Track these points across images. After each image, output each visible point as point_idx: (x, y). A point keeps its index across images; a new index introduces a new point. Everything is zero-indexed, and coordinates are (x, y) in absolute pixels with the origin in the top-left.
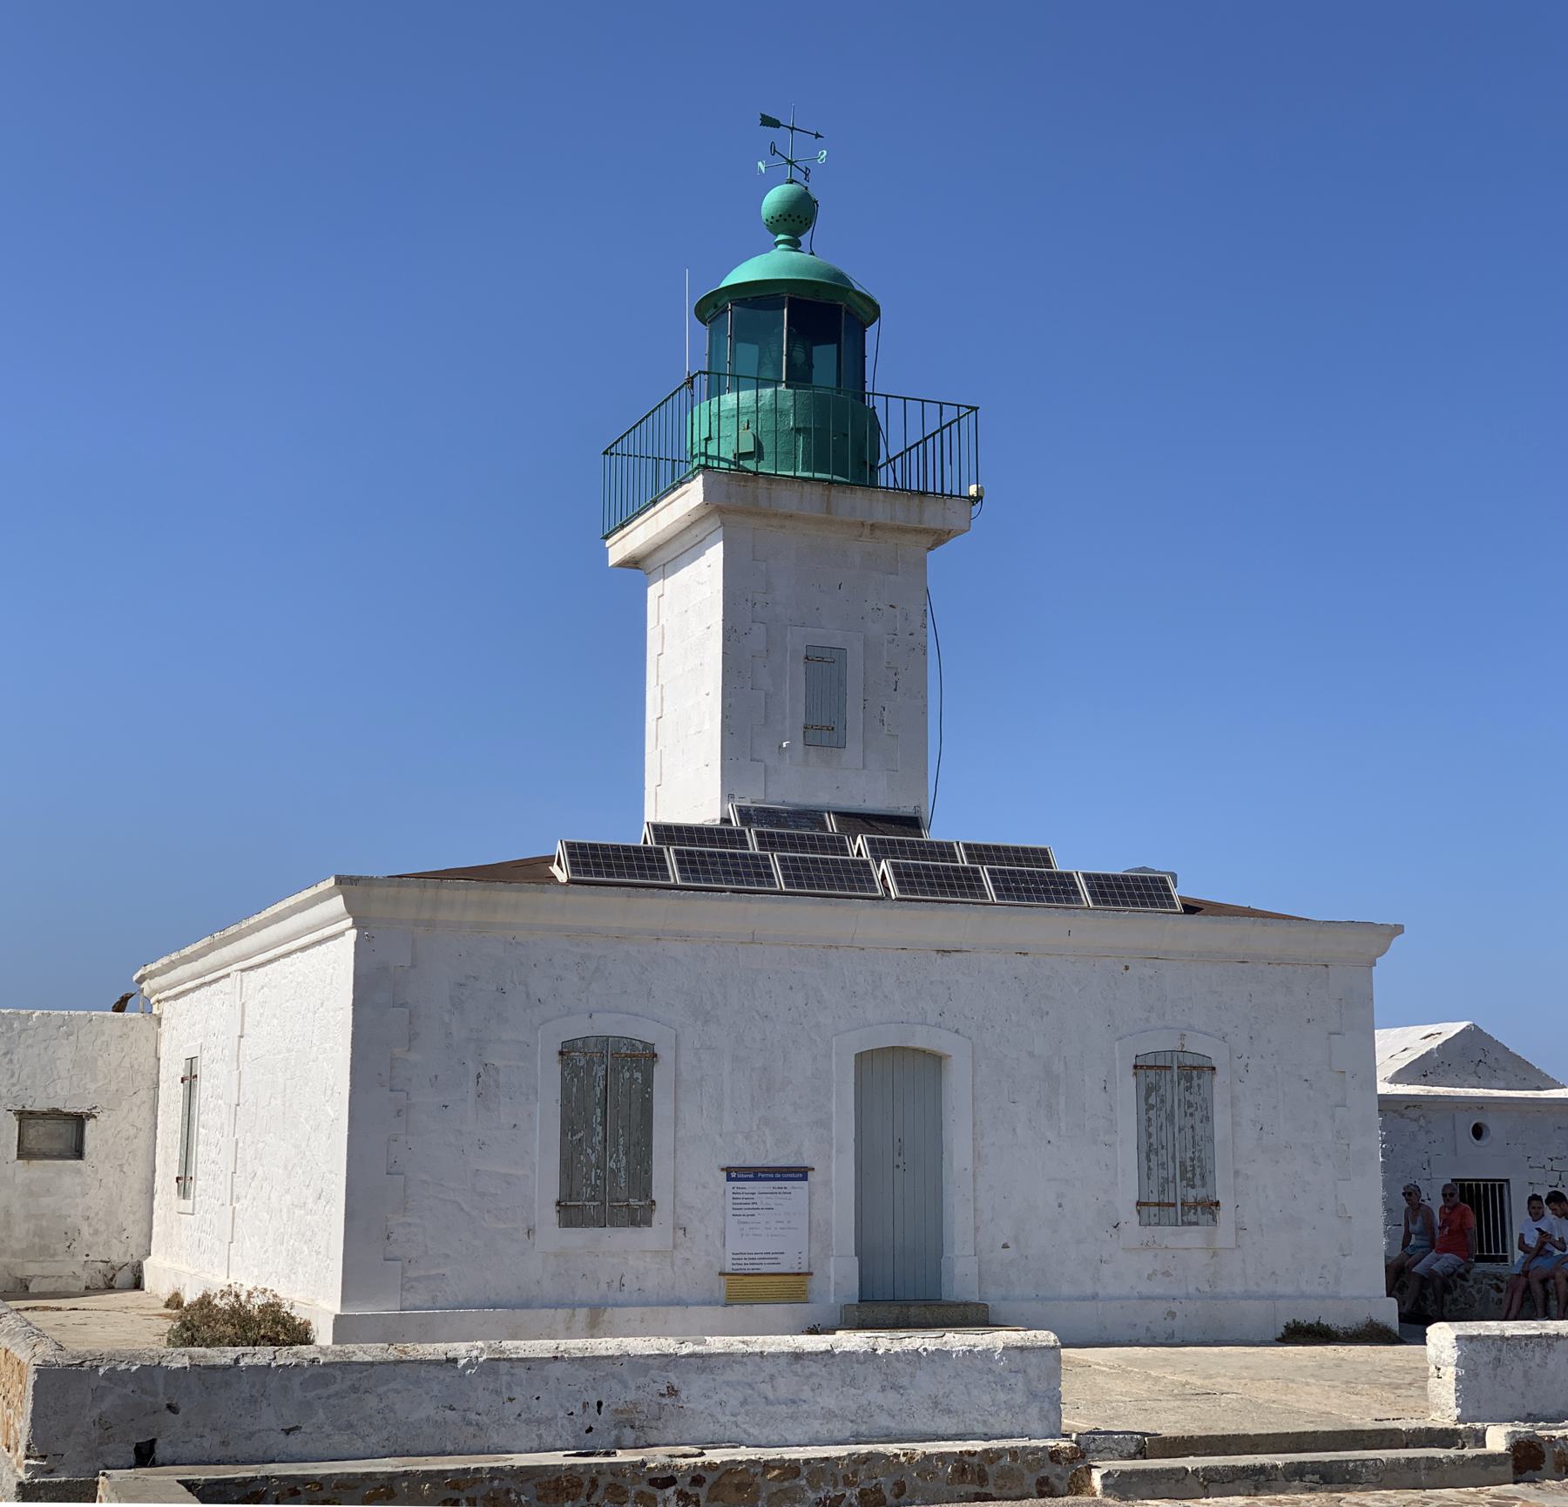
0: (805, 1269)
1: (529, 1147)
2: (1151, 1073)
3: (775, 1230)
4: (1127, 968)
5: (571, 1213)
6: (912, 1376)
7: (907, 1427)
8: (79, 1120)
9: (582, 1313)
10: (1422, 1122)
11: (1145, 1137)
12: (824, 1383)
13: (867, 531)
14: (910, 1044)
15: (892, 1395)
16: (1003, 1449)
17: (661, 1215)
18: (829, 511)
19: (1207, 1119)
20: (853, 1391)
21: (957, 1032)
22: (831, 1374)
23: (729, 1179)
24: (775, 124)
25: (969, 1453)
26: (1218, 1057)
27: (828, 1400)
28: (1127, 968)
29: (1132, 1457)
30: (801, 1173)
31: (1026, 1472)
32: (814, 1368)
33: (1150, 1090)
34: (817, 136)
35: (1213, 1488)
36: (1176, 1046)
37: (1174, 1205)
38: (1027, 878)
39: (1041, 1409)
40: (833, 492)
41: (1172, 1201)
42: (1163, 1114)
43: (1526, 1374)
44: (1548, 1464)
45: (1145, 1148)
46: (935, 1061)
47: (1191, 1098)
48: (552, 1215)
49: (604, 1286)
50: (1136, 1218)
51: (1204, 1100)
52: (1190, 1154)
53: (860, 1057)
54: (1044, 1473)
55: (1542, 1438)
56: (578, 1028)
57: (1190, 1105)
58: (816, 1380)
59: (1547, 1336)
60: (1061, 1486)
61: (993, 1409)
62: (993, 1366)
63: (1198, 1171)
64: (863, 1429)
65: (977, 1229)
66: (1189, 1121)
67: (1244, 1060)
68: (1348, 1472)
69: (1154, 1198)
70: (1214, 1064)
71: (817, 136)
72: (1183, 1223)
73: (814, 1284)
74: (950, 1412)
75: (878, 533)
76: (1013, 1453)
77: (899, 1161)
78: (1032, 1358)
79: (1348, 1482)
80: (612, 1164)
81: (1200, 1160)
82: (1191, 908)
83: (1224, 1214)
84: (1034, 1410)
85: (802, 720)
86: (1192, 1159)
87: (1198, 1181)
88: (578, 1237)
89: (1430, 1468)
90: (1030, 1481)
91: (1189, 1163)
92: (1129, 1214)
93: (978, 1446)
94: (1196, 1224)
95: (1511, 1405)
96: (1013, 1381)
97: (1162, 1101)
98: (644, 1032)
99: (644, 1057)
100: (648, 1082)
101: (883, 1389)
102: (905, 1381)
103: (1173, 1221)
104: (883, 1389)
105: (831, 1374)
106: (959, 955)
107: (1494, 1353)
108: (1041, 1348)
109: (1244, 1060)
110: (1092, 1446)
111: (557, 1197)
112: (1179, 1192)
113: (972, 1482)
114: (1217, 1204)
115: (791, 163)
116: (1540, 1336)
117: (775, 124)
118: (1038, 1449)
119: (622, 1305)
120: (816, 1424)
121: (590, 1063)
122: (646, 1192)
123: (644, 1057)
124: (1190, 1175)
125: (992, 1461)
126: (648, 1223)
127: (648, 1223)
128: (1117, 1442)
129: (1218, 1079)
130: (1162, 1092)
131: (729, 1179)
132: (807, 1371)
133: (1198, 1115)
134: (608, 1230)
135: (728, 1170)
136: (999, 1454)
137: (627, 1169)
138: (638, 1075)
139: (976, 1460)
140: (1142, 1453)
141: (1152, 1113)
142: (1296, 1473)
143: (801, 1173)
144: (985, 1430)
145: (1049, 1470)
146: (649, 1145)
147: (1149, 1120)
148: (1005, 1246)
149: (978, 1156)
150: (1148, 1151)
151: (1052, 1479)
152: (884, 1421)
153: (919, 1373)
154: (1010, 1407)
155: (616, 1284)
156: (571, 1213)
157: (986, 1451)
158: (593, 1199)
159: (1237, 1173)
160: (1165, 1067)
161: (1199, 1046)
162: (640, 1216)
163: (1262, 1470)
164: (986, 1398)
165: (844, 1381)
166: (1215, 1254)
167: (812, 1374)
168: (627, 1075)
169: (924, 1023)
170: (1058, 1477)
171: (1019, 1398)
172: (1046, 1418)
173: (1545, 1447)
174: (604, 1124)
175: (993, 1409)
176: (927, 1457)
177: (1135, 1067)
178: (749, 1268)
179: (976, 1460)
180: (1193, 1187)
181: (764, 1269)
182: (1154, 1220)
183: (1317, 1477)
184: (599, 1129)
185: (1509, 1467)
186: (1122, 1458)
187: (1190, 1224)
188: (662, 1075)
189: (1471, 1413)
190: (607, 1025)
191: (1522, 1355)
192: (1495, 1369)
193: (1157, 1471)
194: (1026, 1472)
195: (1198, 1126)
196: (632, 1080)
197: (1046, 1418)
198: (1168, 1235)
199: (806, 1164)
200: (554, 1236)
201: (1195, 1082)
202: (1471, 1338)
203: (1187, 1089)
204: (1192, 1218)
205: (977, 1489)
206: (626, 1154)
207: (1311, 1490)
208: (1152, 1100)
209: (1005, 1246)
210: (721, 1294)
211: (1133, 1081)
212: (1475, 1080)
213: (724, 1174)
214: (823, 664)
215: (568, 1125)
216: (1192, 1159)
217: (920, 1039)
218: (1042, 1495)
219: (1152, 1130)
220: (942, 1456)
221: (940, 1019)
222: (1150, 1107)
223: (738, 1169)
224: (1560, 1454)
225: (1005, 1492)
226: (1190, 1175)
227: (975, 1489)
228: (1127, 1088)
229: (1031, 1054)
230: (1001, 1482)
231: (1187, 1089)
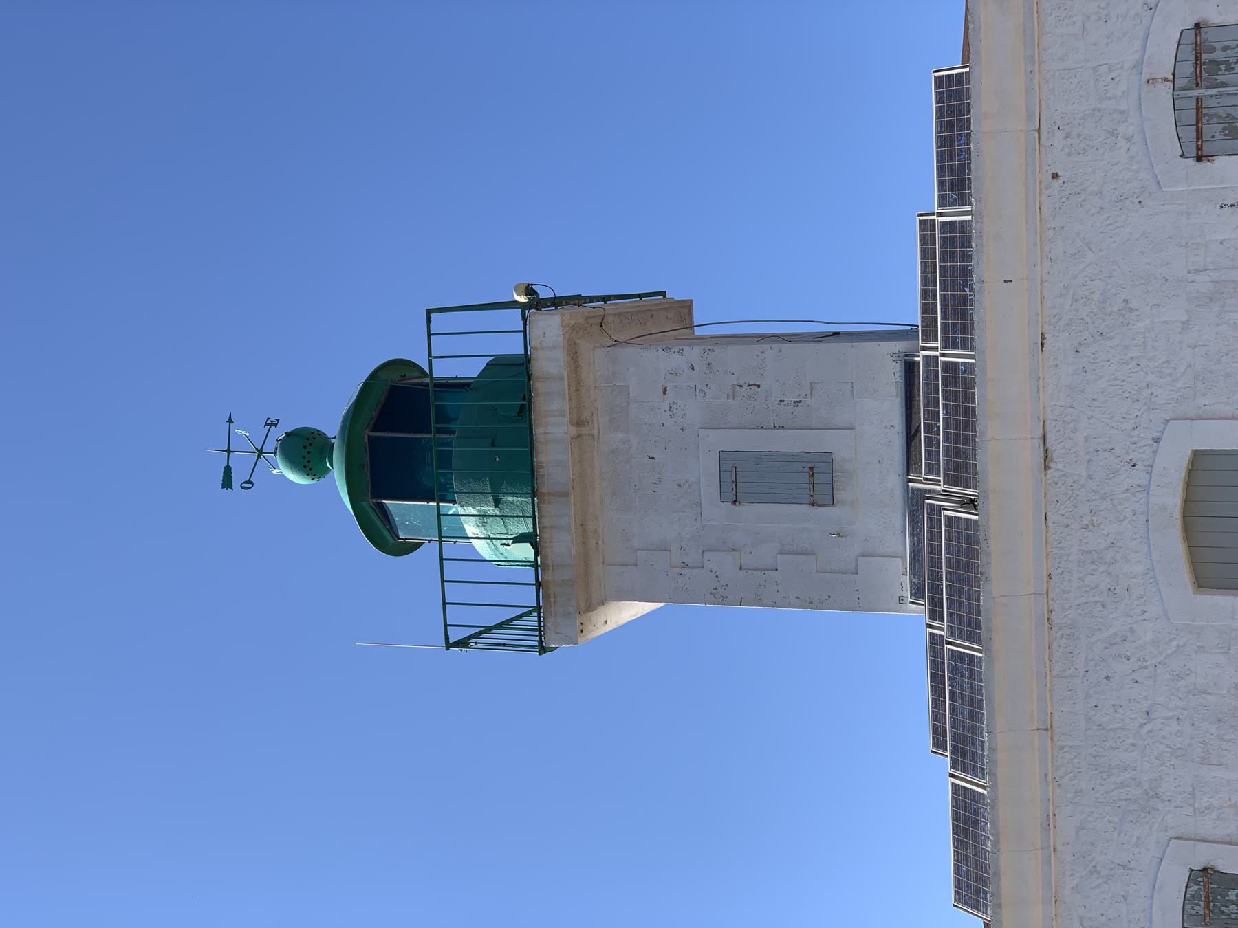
2: (1207, 131)
4: (1055, 176)
8: (1182, 156)
13: (585, 430)
14: (1177, 514)
21: (1157, 441)
28: (1055, 176)
34: (230, 421)
36: (1165, 91)
38: (949, 261)
40: (544, 489)
53: (1203, 582)
70: (1190, 25)
71: (230, 421)
75: (586, 415)
82: (966, 58)
85: (805, 508)
160: (1198, 109)
161: (1164, 52)
168: (1233, 908)
169: (1146, 489)
177: (1199, 159)
201: (1219, 55)
211: (1221, 161)
214: (742, 480)
217: (1172, 498)
221: (1140, 466)
229: (1186, 325)
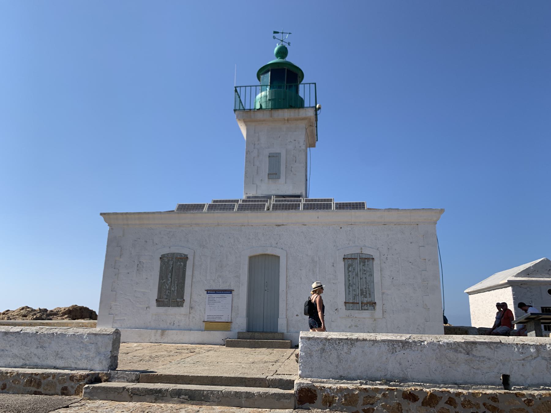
0: (230, 321)
1: (150, 284)
3: (220, 309)
5: (160, 303)
6: (50, 343)
7: (44, 363)
9: (159, 331)
10: (528, 289)
11: (347, 280)
12: (15, 344)
13: (286, 121)
14: (266, 253)
15: (40, 350)
16: (51, 373)
17: (186, 304)
18: (271, 117)
19: (371, 275)
20: (26, 348)
22: (18, 340)
23: (207, 293)
24: (278, 33)
25: (36, 374)
26: (375, 255)
27: (15, 351)
29: (132, 381)
30: (230, 292)
31: (58, 384)
32: (12, 338)
33: (349, 266)
35: (135, 397)
36: (358, 251)
37: (358, 303)
38: (323, 205)
39: (100, 359)
41: (358, 302)
42: (354, 274)
43: (338, 357)
44: (319, 401)
45: (347, 284)
46: (279, 257)
47: (365, 268)
48: (154, 303)
49: (168, 324)
50: (344, 307)
51: (370, 269)
52: (365, 287)
54: (65, 385)
55: (317, 387)
56: (166, 251)
57: (365, 271)
58: (12, 343)
59: (351, 340)
60: (73, 391)
61: (80, 358)
62: (83, 341)
63: (368, 292)
64: (27, 362)
65: (287, 310)
66: (364, 276)
67: (386, 256)
68: (203, 396)
69: (351, 301)
72: (362, 309)
73: (233, 326)
74: (62, 358)
76: (54, 375)
77: (266, 289)
78: (99, 339)
79: (202, 400)
80: (173, 289)
81: (368, 289)
83: (377, 307)
84: (97, 360)
85: (267, 172)
86: (366, 288)
87: (368, 295)
88: (162, 310)
89: (247, 398)
90: (59, 388)
91: (364, 289)
92: (342, 306)
93: (40, 371)
94: (367, 310)
95: (330, 371)
96: (90, 347)
97: (354, 269)
98: (185, 251)
99: (185, 258)
100: (185, 265)
101: (37, 348)
102: (47, 345)
103: (358, 308)
104: (37, 348)
105: (18, 340)
106: (283, 226)
107: (321, 346)
108: (104, 334)
109: (386, 256)
110: (116, 376)
111: (156, 298)
112: (359, 299)
113: (33, 386)
114: (375, 303)
115: (282, 41)
116: (347, 339)
117: (278, 33)
118: (65, 374)
119: (172, 330)
120: (9, 359)
121: (169, 261)
122: (182, 297)
123: (185, 258)
124: (365, 293)
125: (44, 378)
126: (182, 306)
127: (182, 306)
128: (127, 375)
129: (375, 262)
130: (354, 266)
131: (207, 293)
132: (9, 339)
133: (368, 274)
134: (170, 308)
135: (207, 291)
136: (48, 375)
137: (177, 290)
138: (182, 263)
139: (38, 377)
140: (138, 380)
141: (350, 273)
142: (178, 393)
143: (230, 292)
144: (76, 366)
145: (68, 384)
146: (184, 283)
147: (349, 275)
148: (297, 315)
149: (287, 286)
150: (349, 286)
151: (69, 388)
152: (36, 360)
153: (53, 342)
154: (87, 357)
155: (172, 324)
156: (160, 303)
157: (43, 374)
158: (166, 299)
159: (383, 293)
160: (355, 259)
161: (367, 252)
162: (179, 303)
163: (160, 391)
164: (78, 353)
165: (22, 344)
166: (375, 320)
167: (11, 340)
169: (271, 246)
170: (72, 387)
171: (92, 354)
172: (101, 362)
173: (318, 392)
174: (171, 278)
175: (80, 358)
176: (18, 374)
178: (212, 320)
179: (38, 377)
180: (366, 297)
181: (217, 320)
182: (351, 308)
183: (187, 397)
184: (170, 279)
185: (293, 400)
186: (128, 381)
187: (365, 310)
188: (189, 264)
189: (307, 373)
190: (174, 250)
191: (337, 348)
192: (321, 353)
193: (110, 388)
194: (58, 384)
195: (368, 277)
196: (181, 265)
197: (101, 362)
198: (357, 314)
199: (232, 289)
200: (154, 309)
201: (367, 263)
202: (309, 339)
203: (363, 265)
204: (366, 308)
205: (36, 389)
206: (177, 286)
207: (183, 403)
208: (350, 269)
209: (297, 315)
210: (203, 328)
211: (343, 263)
212: (548, 276)
213: (206, 292)
214: (274, 158)
215: (161, 278)
216: (366, 288)
217: (269, 251)
218: (63, 394)
219: (350, 279)
220: (24, 375)
222: (349, 271)
223: (210, 290)
224: (326, 396)
225: (47, 392)
226: (365, 293)
227: (34, 389)
228: (341, 265)
229: (307, 255)
230: (46, 387)
231: (363, 265)
